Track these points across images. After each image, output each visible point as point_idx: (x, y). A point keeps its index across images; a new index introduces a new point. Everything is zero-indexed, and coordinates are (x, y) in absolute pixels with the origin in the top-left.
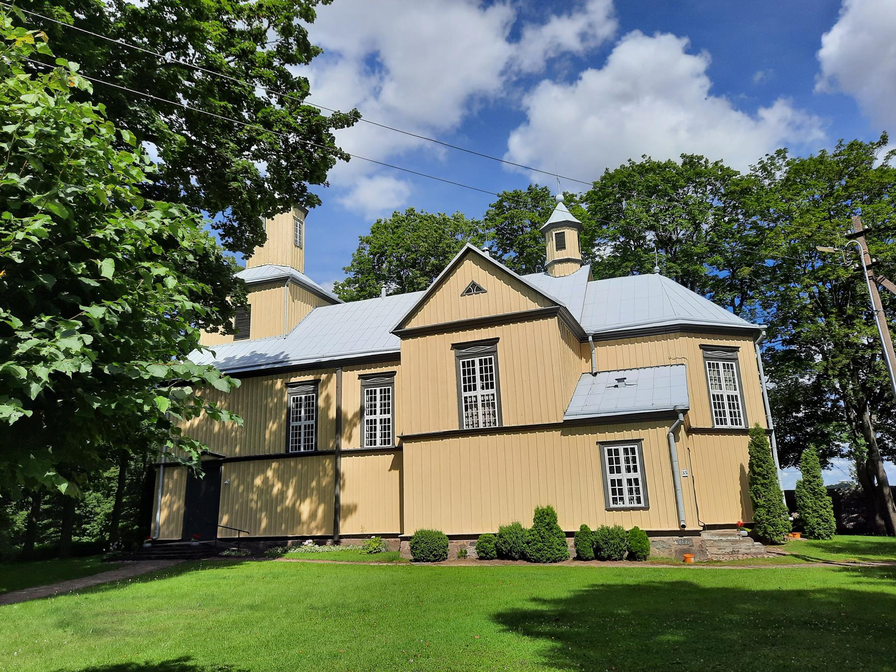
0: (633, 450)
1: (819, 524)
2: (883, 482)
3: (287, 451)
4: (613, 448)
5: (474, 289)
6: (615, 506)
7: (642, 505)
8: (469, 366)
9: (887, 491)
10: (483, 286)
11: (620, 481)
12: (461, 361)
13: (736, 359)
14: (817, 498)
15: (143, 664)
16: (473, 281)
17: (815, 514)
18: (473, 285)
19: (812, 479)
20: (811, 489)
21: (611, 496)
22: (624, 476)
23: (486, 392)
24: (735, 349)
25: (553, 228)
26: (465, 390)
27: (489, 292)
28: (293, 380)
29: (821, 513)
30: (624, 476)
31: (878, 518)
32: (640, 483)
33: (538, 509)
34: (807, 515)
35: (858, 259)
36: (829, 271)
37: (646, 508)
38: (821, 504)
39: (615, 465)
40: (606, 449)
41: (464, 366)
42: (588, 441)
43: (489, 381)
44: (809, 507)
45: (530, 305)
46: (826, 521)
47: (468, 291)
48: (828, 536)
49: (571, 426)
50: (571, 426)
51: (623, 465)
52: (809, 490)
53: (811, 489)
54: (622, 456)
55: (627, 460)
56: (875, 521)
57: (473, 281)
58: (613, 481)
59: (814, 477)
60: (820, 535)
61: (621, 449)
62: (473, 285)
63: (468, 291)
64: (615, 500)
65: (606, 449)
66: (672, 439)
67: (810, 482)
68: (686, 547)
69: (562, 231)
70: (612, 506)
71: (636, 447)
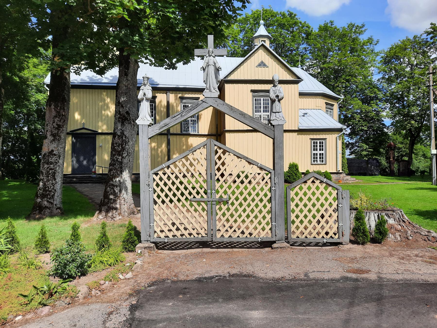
0: (322, 143)
3: (181, 131)
4: (315, 141)
5: (262, 64)
6: (314, 163)
7: (324, 163)
8: (258, 101)
10: (267, 64)
12: (255, 98)
13: (332, 109)
16: (262, 61)
18: (262, 62)
21: (313, 160)
22: (318, 152)
23: (265, 113)
24: (333, 105)
25: (260, 37)
26: (256, 112)
27: (269, 67)
28: (186, 96)
30: (318, 152)
32: (324, 155)
33: (291, 163)
37: (325, 164)
40: (313, 141)
41: (256, 101)
42: (306, 138)
43: (267, 109)
45: (289, 77)
47: (259, 65)
49: (301, 131)
50: (301, 131)
51: (318, 148)
54: (318, 145)
55: (320, 146)
57: (262, 61)
61: (318, 141)
62: (262, 62)
63: (259, 65)
64: (314, 161)
65: (313, 141)
66: (338, 139)
68: (338, 178)
69: (265, 40)
70: (313, 163)
71: (324, 141)
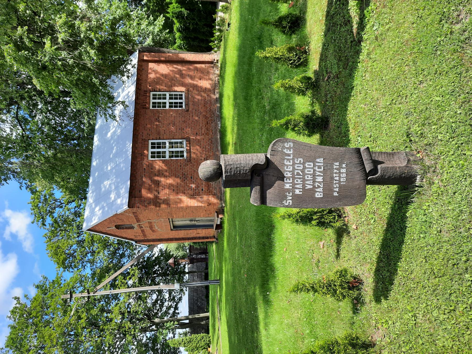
1: (204, 341)
2: (187, 318)
9: (190, 317)
11: (170, 103)
14: (192, 341)
15: (23, 246)
17: (200, 342)
19: (184, 342)
20: (188, 343)
29: (199, 339)
31: (202, 323)
34: (200, 346)
35: (84, 297)
36: (80, 326)
38: (195, 339)
39: (157, 97)
44: (196, 345)
46: (203, 337)
48: (209, 337)
52: (188, 344)
53: (188, 343)
56: (203, 324)
58: (170, 107)
59: (182, 341)
60: (209, 341)
67: (185, 343)
